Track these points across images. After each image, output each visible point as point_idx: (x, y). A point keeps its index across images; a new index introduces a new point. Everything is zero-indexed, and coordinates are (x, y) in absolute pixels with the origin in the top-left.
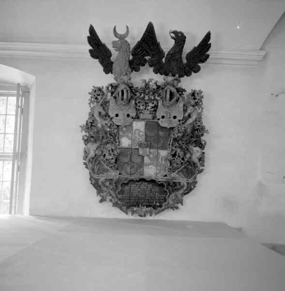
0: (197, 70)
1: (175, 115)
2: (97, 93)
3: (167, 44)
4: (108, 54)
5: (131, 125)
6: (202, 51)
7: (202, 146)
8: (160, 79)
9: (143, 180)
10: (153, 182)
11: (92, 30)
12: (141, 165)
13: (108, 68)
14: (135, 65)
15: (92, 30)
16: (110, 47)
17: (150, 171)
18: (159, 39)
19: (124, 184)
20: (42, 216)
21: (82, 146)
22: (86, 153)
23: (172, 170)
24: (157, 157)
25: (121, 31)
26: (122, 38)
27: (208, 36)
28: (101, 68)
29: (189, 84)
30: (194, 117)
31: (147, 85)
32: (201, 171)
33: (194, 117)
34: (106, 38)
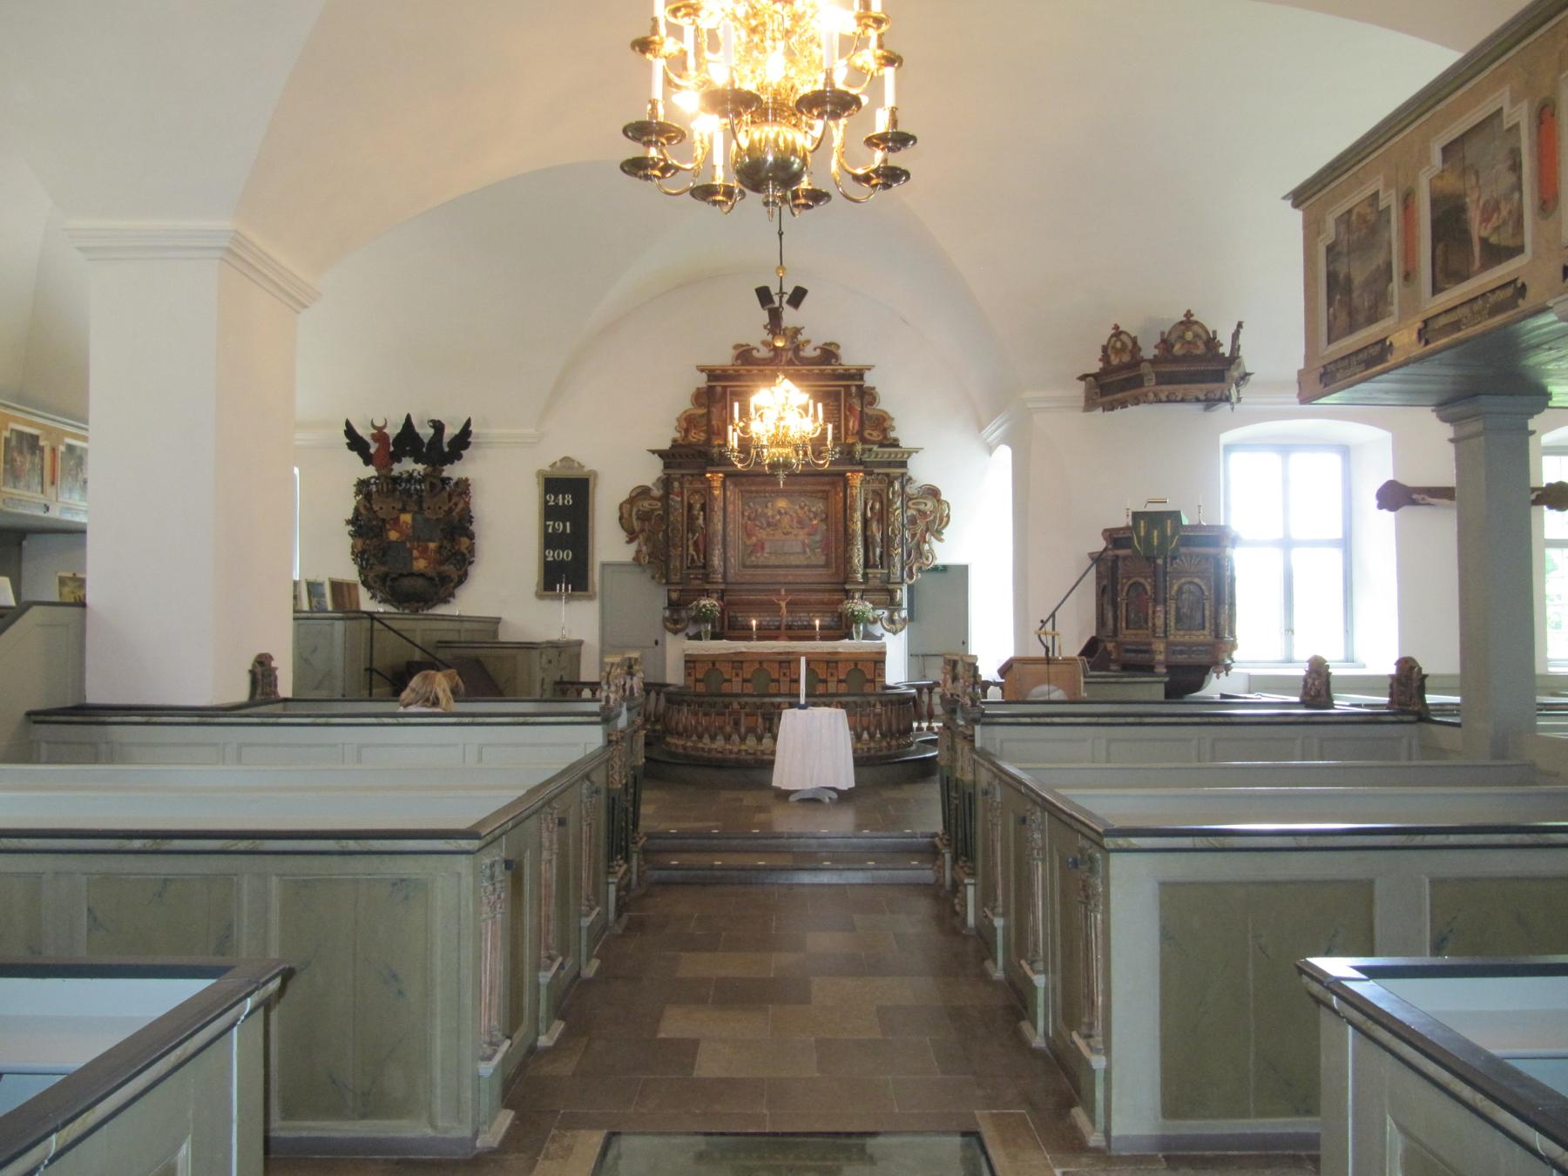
0: (459, 457)
1: (547, 458)
2: (362, 485)
3: (426, 432)
4: (367, 446)
5: (398, 518)
6: (463, 439)
7: (471, 536)
8: (420, 467)
9: (412, 574)
10: (422, 575)
11: (348, 424)
12: (412, 559)
13: (368, 460)
14: (396, 457)
15: (348, 424)
16: (368, 439)
17: (420, 565)
18: (418, 430)
19: (394, 580)
20: (685, 883)
21: (350, 541)
22: (353, 547)
23: (441, 563)
24: (426, 549)
25: (379, 424)
26: (380, 429)
27: (468, 423)
28: (360, 461)
29: (453, 471)
30: (461, 505)
31: (411, 475)
32: (471, 563)
33: (461, 505)
34: (364, 432)
